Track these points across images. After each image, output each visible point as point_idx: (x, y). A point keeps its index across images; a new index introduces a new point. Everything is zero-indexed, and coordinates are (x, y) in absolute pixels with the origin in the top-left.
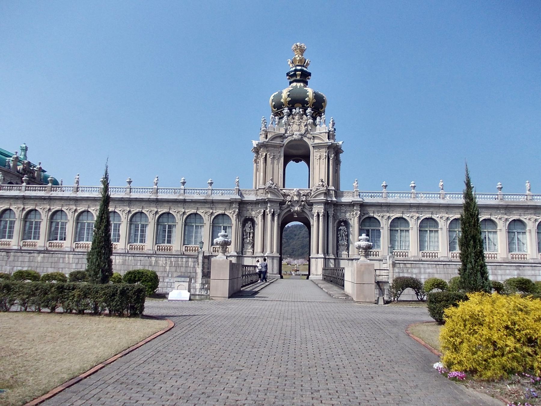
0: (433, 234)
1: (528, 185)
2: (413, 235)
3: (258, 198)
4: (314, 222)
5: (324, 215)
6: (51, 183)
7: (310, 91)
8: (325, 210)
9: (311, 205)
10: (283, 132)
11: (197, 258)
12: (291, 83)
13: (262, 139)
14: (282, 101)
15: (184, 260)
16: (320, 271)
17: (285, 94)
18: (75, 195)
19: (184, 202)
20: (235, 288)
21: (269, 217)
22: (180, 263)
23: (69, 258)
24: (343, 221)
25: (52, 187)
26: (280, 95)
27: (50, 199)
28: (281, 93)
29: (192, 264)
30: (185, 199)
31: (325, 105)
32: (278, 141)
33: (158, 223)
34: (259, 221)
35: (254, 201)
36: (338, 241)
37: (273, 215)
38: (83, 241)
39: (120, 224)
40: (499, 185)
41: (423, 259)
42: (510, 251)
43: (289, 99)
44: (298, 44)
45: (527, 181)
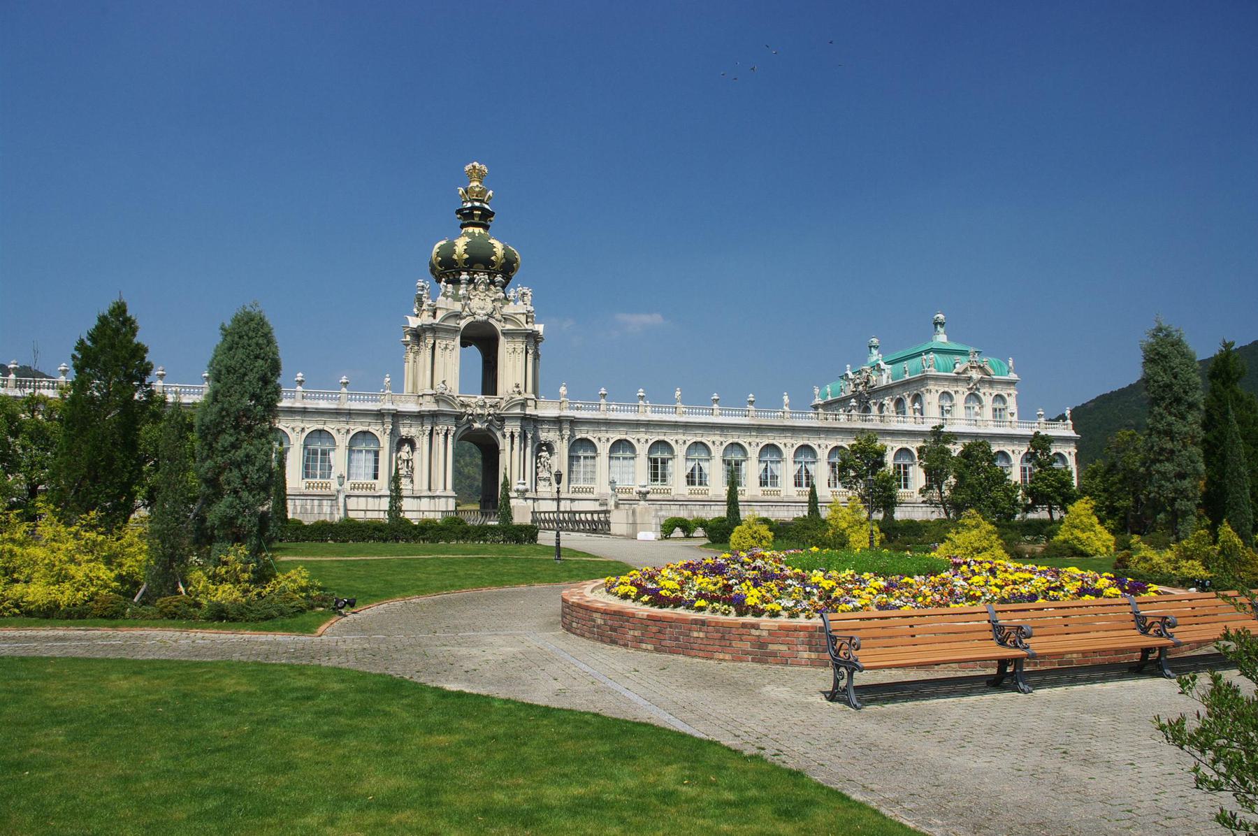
0: (589, 462)
1: (786, 399)
3: (423, 409)
4: (504, 444)
5: (520, 436)
6: (15, 374)
7: (498, 247)
9: (502, 419)
11: (337, 498)
12: (462, 226)
13: (426, 319)
14: (455, 257)
15: (316, 503)
17: (461, 245)
20: (707, 541)
22: (309, 507)
24: (545, 444)
25: (17, 381)
26: (451, 246)
29: (329, 509)
30: (305, 408)
31: (518, 266)
32: (451, 323)
34: (422, 443)
35: (414, 412)
36: (537, 474)
37: (446, 435)
38: (695, 484)
42: (307, 475)
43: (466, 256)
44: (476, 164)
45: (388, 375)
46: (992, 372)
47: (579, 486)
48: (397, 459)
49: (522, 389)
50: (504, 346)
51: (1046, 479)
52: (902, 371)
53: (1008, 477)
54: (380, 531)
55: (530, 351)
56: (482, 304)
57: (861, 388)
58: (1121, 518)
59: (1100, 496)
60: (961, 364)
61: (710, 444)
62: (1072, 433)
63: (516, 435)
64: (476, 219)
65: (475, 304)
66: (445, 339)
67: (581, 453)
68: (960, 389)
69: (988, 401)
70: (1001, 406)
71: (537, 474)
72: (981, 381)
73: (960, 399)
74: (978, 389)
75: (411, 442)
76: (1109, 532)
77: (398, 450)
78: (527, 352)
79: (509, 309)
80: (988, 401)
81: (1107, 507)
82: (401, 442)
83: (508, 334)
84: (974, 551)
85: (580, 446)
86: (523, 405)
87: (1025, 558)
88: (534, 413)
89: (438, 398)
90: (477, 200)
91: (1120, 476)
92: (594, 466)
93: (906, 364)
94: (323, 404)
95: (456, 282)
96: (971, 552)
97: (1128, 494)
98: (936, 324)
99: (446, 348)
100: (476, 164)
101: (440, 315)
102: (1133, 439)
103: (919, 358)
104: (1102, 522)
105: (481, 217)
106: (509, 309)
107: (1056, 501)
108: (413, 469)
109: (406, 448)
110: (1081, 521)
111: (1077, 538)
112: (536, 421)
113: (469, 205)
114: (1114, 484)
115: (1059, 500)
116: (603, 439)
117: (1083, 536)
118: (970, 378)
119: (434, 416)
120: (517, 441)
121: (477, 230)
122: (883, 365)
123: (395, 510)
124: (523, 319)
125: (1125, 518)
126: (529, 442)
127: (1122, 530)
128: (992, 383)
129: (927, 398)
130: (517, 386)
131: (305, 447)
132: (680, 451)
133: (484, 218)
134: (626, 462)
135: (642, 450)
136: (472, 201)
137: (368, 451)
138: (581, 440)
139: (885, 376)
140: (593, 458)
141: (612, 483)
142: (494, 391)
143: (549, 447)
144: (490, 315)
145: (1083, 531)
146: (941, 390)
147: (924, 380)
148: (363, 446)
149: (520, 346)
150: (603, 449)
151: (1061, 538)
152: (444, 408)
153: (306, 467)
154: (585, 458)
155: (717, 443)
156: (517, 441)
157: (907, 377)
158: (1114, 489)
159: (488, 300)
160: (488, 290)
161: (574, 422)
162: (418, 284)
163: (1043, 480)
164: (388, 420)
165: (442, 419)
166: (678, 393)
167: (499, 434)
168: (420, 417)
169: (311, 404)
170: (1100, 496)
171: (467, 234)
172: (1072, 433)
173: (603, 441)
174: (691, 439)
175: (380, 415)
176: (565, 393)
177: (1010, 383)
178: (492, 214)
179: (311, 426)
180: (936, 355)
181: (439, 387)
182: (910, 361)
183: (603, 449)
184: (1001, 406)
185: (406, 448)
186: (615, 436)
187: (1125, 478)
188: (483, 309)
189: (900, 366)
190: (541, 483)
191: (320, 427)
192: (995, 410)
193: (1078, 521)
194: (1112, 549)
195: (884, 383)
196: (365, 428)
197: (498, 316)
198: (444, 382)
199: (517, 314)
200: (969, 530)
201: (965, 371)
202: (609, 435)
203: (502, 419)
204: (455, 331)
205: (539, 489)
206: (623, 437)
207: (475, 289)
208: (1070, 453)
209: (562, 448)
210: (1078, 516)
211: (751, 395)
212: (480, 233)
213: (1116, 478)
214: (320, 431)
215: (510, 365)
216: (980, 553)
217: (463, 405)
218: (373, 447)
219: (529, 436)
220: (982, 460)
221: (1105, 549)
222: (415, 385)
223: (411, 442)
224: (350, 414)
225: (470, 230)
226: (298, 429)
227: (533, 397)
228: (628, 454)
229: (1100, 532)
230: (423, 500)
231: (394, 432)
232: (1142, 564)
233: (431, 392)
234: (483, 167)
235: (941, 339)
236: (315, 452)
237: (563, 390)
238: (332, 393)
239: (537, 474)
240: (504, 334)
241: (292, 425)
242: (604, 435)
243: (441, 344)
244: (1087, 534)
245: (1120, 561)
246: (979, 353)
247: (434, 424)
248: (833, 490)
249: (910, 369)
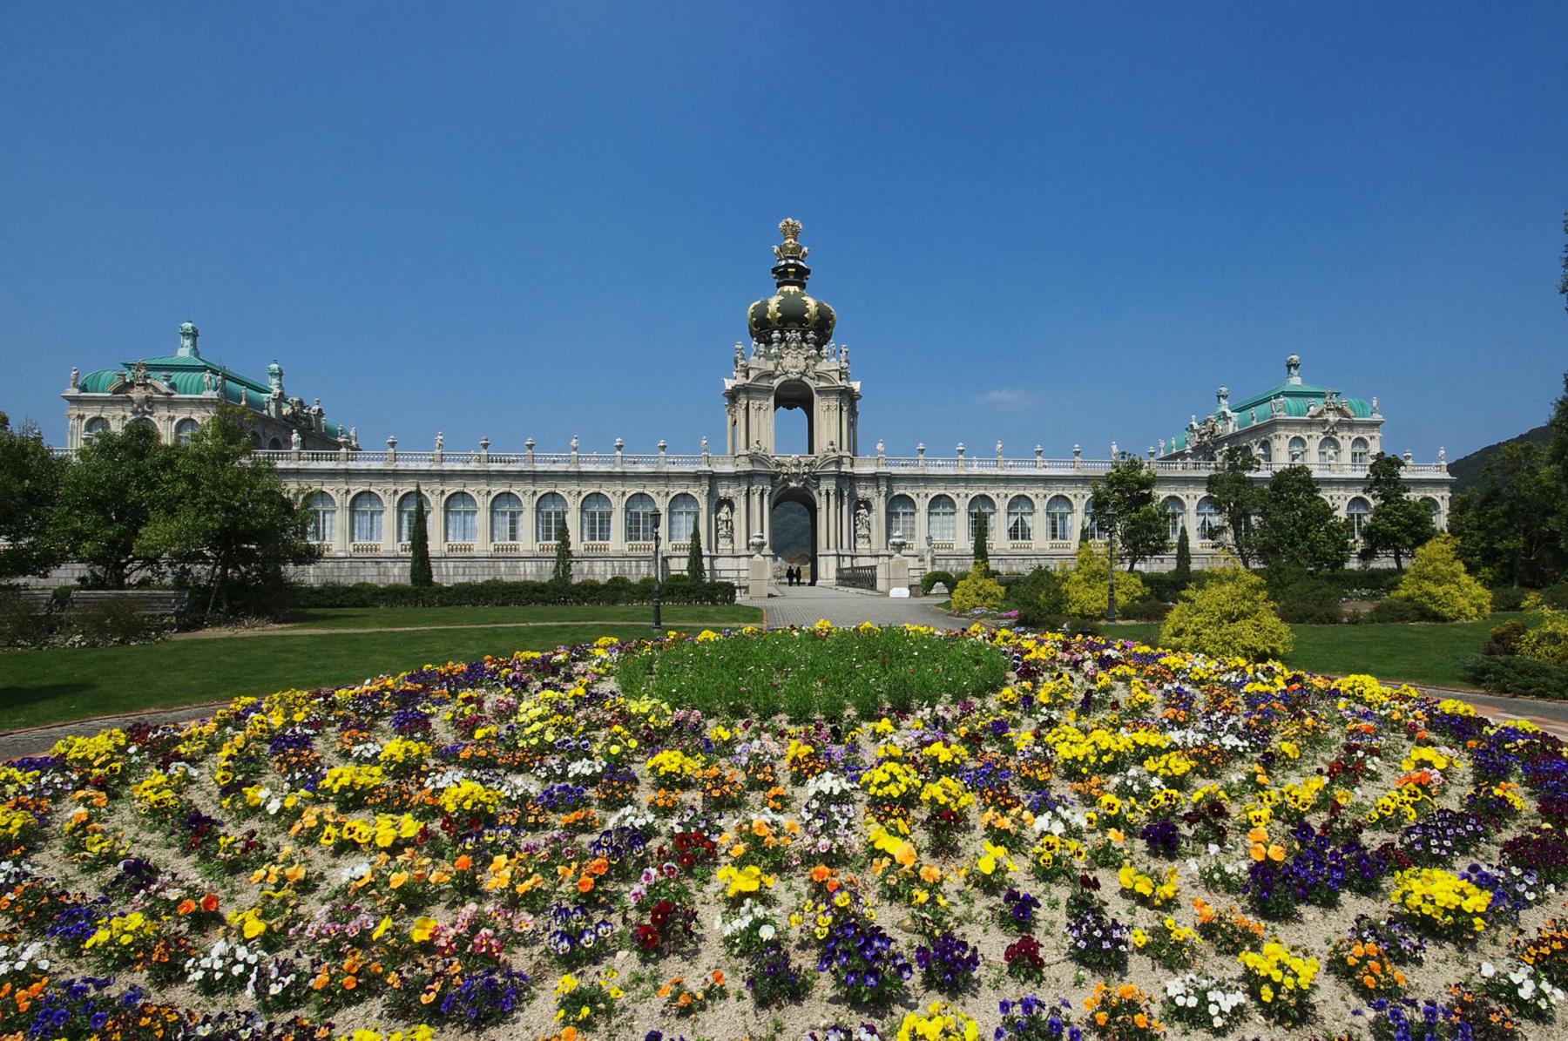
0: (908, 518)
2: (482, 518)
4: (821, 503)
5: (835, 494)
7: (811, 303)
8: (837, 485)
9: (818, 478)
10: (772, 369)
12: (779, 285)
13: (740, 380)
14: (769, 316)
16: (833, 574)
17: (773, 303)
18: (439, 468)
19: (624, 477)
21: (756, 498)
23: (447, 567)
24: (863, 502)
27: (349, 474)
28: (767, 304)
31: (834, 323)
32: (764, 383)
33: (538, 509)
34: (740, 504)
37: (762, 495)
39: (564, 513)
40: (618, 441)
41: (451, 554)
43: (779, 315)
44: (789, 220)
46: (1352, 414)
48: (716, 520)
49: (837, 446)
50: (819, 404)
51: (1391, 514)
52: (1250, 417)
53: (1335, 513)
54: (542, 592)
55: (845, 409)
56: (794, 362)
57: (1206, 438)
58: (1504, 565)
59: (1472, 535)
60: (1316, 406)
61: (1033, 498)
62: (1446, 476)
63: (832, 493)
64: (791, 277)
65: (788, 362)
66: (759, 399)
67: (900, 510)
68: (1314, 433)
69: (1346, 446)
70: (1363, 450)
71: (855, 531)
72: (1339, 424)
73: (1313, 446)
74: (1334, 433)
75: (729, 503)
76: (1484, 585)
77: (718, 511)
78: (841, 410)
79: (822, 366)
80: (1346, 446)
81: (1483, 549)
82: (718, 503)
84: (1224, 617)
85: (898, 505)
86: (839, 462)
87: (1341, 623)
88: (850, 470)
89: (753, 459)
91: (1505, 506)
92: (914, 522)
93: (1253, 411)
94: (642, 468)
96: (1220, 621)
97: (1517, 531)
98: (1290, 366)
99: (760, 408)
100: (789, 220)
101: (752, 374)
102: (1527, 455)
103: (1268, 404)
104: (1471, 570)
105: (795, 274)
106: (822, 366)
107: (1404, 543)
108: (732, 528)
109: (726, 509)
110: (1435, 568)
111: (1428, 594)
112: (853, 479)
113: (783, 263)
114: (1494, 518)
115: (1410, 542)
116: (922, 495)
117: (1439, 591)
118: (1326, 421)
119: (749, 477)
120: (832, 498)
121: (793, 289)
122: (1229, 413)
123: (421, 559)
124: (836, 376)
125: (1510, 565)
126: (846, 499)
127: (1504, 581)
128: (1351, 426)
129: (1276, 444)
130: (832, 444)
131: (627, 510)
132: (1001, 505)
133: (800, 276)
134: (946, 518)
135: (962, 505)
136: (787, 258)
137: (688, 513)
138: (901, 496)
139: (1231, 424)
140: (913, 514)
141: (929, 538)
142: (811, 451)
143: (868, 505)
144: (803, 374)
145: (1438, 583)
146: (1292, 435)
147: (1272, 425)
148: (683, 509)
149: (834, 402)
150: (922, 505)
151: (1403, 593)
152: (759, 468)
154: (904, 514)
155: (1041, 496)
156: (832, 498)
157: (1255, 423)
158: (1494, 525)
159: (801, 358)
160: (801, 348)
161: (891, 479)
163: (1386, 515)
164: (705, 482)
165: (756, 479)
167: (815, 493)
168: (736, 478)
169: (630, 468)
170: (1472, 535)
171: (782, 293)
172: (1446, 476)
173: (922, 498)
174: (1013, 493)
175: (697, 477)
177: (1374, 425)
178: (808, 272)
179: (632, 490)
180: (1288, 399)
181: (753, 447)
182: (1259, 407)
183: (922, 505)
184: (1363, 450)
185: (726, 509)
186: (934, 492)
187: (1512, 510)
188: (796, 367)
189: (1248, 413)
190: (860, 541)
191: (640, 490)
193: (1430, 568)
194: (1487, 612)
195: (1231, 431)
196: (684, 491)
197: (811, 374)
200: (1221, 583)
201: (1320, 414)
202: (928, 491)
203: (818, 478)
204: (769, 390)
205: (858, 546)
206: (942, 492)
207: (787, 347)
208: (1442, 498)
209: (879, 505)
210: (1431, 561)
213: (1498, 510)
214: (642, 494)
215: (824, 426)
216: (1234, 621)
217: (779, 465)
218: (692, 509)
219: (846, 493)
220: (1297, 492)
221: (1474, 610)
222: (734, 446)
223: (729, 503)
224: (669, 477)
225: (786, 288)
226: (619, 493)
227: (848, 454)
228: (948, 510)
229: (1467, 586)
230: (742, 559)
231: (711, 494)
232: (1547, 648)
233: (746, 452)
234: (797, 222)
235: (1295, 382)
236: (637, 514)
237: (880, 446)
239: (855, 531)
240: (818, 392)
241: (613, 489)
242: (923, 491)
243: (754, 404)
244: (1446, 587)
245: (1498, 638)
246: (1338, 394)
247: (750, 484)
249: (1258, 416)
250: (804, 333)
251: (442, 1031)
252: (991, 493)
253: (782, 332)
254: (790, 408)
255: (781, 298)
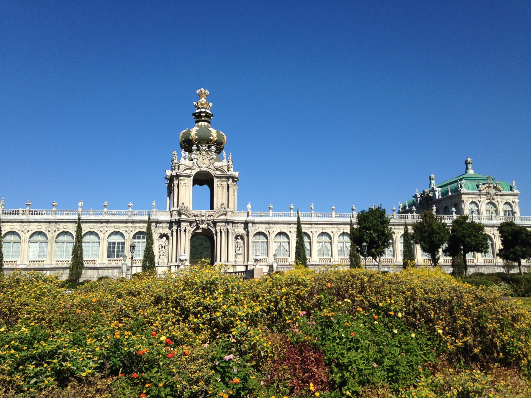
7: (214, 133)
12: (196, 122)
17: (194, 131)
32: (188, 172)
45: (154, 201)
46: (502, 189)
47: (489, 259)
83: (219, 177)
90: (203, 108)
95: (190, 151)
100: (202, 89)
113: (199, 111)
120: (223, 234)
142: (212, 208)
153: (109, 252)
162: (173, 153)
166: (312, 206)
176: (250, 208)
192: (506, 211)
198: (183, 204)
199: (222, 166)
211: (292, 205)
212: (205, 125)
225: (200, 123)
238: (63, 211)
248: (484, 259)
250: (209, 147)
251: (394, 233)
252: (122, 230)
253: (197, 146)
254: (201, 185)
255: (197, 128)
